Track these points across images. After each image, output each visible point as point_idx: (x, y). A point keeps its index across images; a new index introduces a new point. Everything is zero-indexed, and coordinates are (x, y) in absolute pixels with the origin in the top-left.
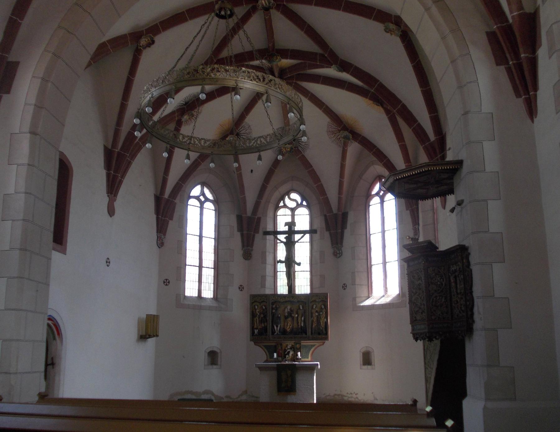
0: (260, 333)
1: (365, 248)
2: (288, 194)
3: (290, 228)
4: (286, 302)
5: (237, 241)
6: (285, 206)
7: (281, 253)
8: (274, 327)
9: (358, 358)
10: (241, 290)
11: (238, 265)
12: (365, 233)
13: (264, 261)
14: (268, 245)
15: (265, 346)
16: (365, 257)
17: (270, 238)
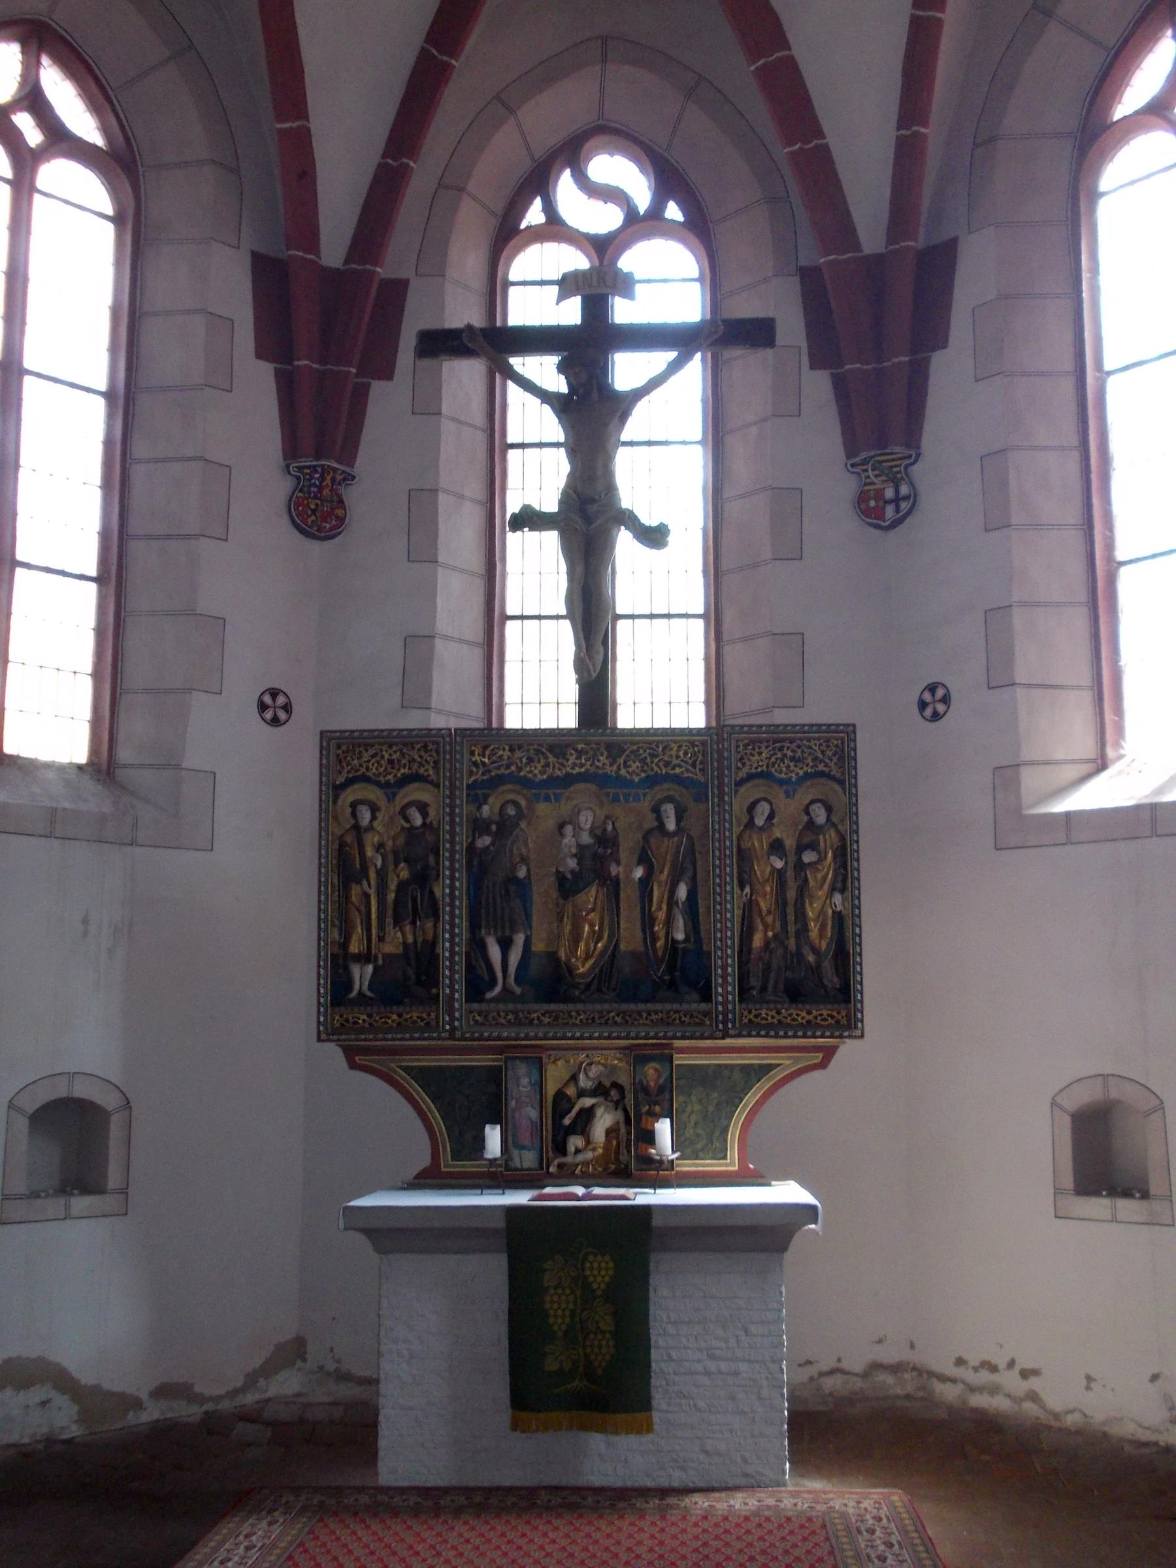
0: (389, 992)
1: (1076, 455)
2: (572, 152)
3: (596, 307)
4: (568, 780)
5: (248, 417)
6: (555, 229)
7: (538, 476)
8: (482, 947)
9: (1038, 1149)
10: (275, 722)
11: (252, 568)
12: (1069, 365)
13: (422, 546)
14: (447, 449)
15: (424, 1077)
16: (1073, 515)
17: (463, 376)
